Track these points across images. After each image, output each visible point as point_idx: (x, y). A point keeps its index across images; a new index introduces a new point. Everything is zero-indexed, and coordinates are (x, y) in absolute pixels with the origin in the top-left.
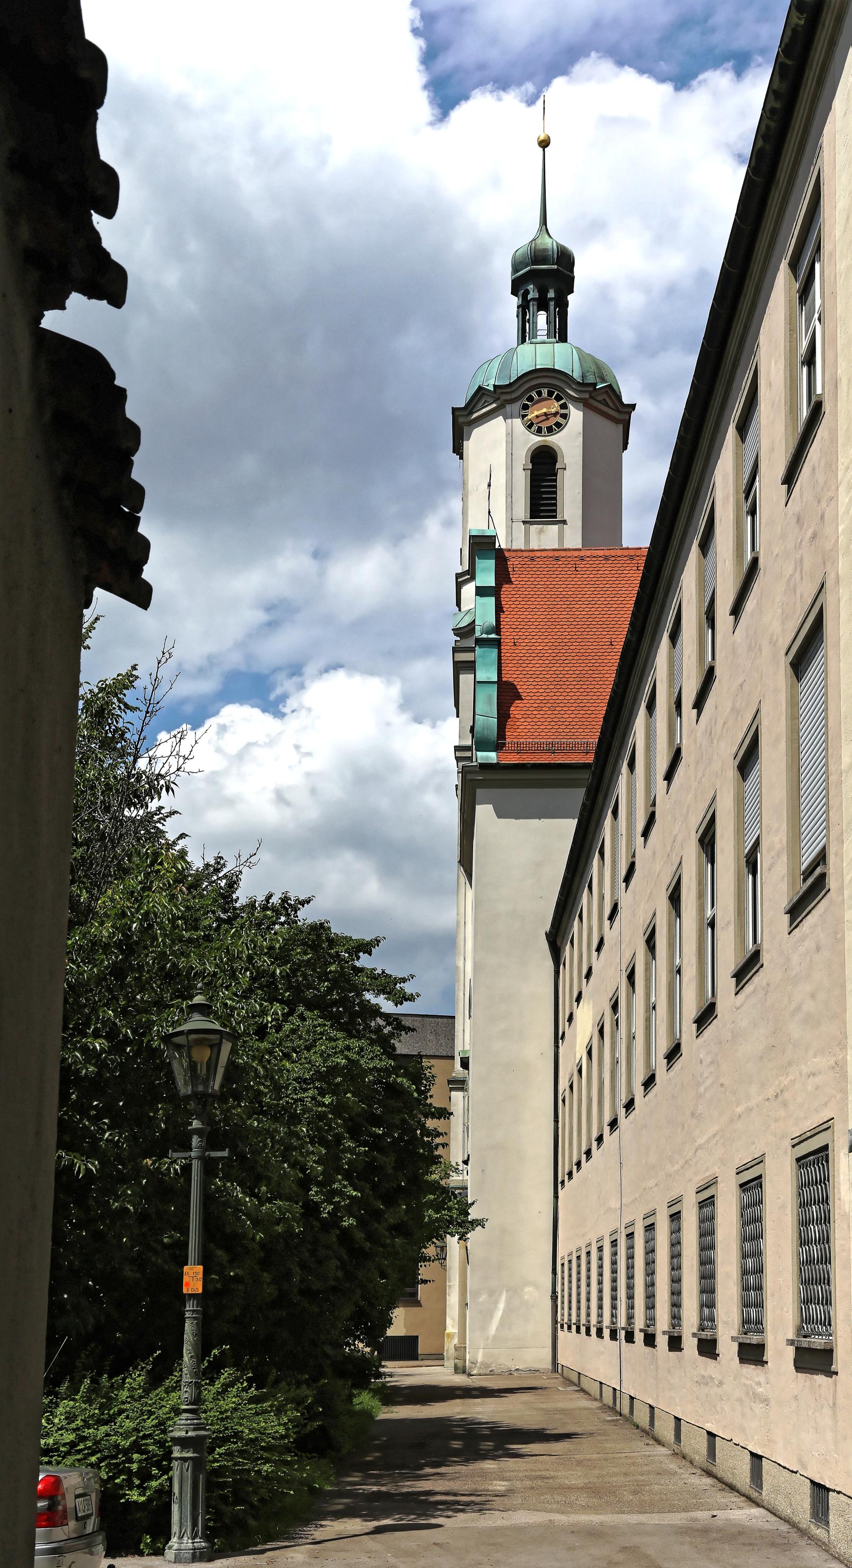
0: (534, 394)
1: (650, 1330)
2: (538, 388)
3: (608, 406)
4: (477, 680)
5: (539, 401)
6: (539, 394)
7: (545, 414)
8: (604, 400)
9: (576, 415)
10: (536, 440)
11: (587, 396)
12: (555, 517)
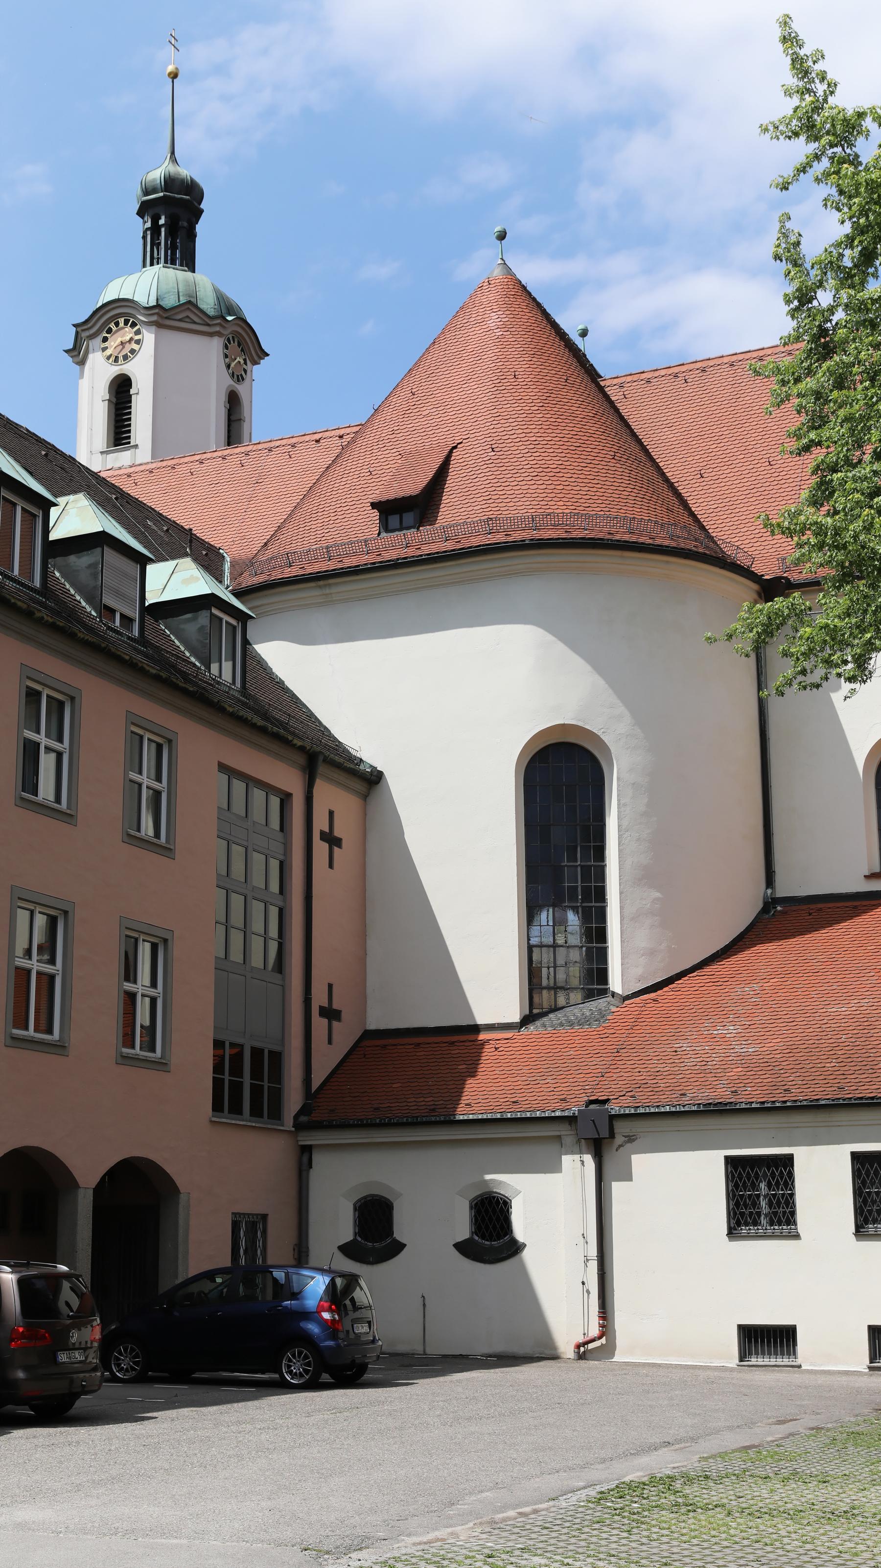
0: (112, 325)
1: (588, 1355)
2: (115, 319)
3: (195, 323)
4: (398, 527)
5: (116, 331)
6: (117, 324)
7: (122, 343)
8: (188, 317)
9: (149, 337)
10: (114, 371)
11: (155, 318)
12: (129, 443)
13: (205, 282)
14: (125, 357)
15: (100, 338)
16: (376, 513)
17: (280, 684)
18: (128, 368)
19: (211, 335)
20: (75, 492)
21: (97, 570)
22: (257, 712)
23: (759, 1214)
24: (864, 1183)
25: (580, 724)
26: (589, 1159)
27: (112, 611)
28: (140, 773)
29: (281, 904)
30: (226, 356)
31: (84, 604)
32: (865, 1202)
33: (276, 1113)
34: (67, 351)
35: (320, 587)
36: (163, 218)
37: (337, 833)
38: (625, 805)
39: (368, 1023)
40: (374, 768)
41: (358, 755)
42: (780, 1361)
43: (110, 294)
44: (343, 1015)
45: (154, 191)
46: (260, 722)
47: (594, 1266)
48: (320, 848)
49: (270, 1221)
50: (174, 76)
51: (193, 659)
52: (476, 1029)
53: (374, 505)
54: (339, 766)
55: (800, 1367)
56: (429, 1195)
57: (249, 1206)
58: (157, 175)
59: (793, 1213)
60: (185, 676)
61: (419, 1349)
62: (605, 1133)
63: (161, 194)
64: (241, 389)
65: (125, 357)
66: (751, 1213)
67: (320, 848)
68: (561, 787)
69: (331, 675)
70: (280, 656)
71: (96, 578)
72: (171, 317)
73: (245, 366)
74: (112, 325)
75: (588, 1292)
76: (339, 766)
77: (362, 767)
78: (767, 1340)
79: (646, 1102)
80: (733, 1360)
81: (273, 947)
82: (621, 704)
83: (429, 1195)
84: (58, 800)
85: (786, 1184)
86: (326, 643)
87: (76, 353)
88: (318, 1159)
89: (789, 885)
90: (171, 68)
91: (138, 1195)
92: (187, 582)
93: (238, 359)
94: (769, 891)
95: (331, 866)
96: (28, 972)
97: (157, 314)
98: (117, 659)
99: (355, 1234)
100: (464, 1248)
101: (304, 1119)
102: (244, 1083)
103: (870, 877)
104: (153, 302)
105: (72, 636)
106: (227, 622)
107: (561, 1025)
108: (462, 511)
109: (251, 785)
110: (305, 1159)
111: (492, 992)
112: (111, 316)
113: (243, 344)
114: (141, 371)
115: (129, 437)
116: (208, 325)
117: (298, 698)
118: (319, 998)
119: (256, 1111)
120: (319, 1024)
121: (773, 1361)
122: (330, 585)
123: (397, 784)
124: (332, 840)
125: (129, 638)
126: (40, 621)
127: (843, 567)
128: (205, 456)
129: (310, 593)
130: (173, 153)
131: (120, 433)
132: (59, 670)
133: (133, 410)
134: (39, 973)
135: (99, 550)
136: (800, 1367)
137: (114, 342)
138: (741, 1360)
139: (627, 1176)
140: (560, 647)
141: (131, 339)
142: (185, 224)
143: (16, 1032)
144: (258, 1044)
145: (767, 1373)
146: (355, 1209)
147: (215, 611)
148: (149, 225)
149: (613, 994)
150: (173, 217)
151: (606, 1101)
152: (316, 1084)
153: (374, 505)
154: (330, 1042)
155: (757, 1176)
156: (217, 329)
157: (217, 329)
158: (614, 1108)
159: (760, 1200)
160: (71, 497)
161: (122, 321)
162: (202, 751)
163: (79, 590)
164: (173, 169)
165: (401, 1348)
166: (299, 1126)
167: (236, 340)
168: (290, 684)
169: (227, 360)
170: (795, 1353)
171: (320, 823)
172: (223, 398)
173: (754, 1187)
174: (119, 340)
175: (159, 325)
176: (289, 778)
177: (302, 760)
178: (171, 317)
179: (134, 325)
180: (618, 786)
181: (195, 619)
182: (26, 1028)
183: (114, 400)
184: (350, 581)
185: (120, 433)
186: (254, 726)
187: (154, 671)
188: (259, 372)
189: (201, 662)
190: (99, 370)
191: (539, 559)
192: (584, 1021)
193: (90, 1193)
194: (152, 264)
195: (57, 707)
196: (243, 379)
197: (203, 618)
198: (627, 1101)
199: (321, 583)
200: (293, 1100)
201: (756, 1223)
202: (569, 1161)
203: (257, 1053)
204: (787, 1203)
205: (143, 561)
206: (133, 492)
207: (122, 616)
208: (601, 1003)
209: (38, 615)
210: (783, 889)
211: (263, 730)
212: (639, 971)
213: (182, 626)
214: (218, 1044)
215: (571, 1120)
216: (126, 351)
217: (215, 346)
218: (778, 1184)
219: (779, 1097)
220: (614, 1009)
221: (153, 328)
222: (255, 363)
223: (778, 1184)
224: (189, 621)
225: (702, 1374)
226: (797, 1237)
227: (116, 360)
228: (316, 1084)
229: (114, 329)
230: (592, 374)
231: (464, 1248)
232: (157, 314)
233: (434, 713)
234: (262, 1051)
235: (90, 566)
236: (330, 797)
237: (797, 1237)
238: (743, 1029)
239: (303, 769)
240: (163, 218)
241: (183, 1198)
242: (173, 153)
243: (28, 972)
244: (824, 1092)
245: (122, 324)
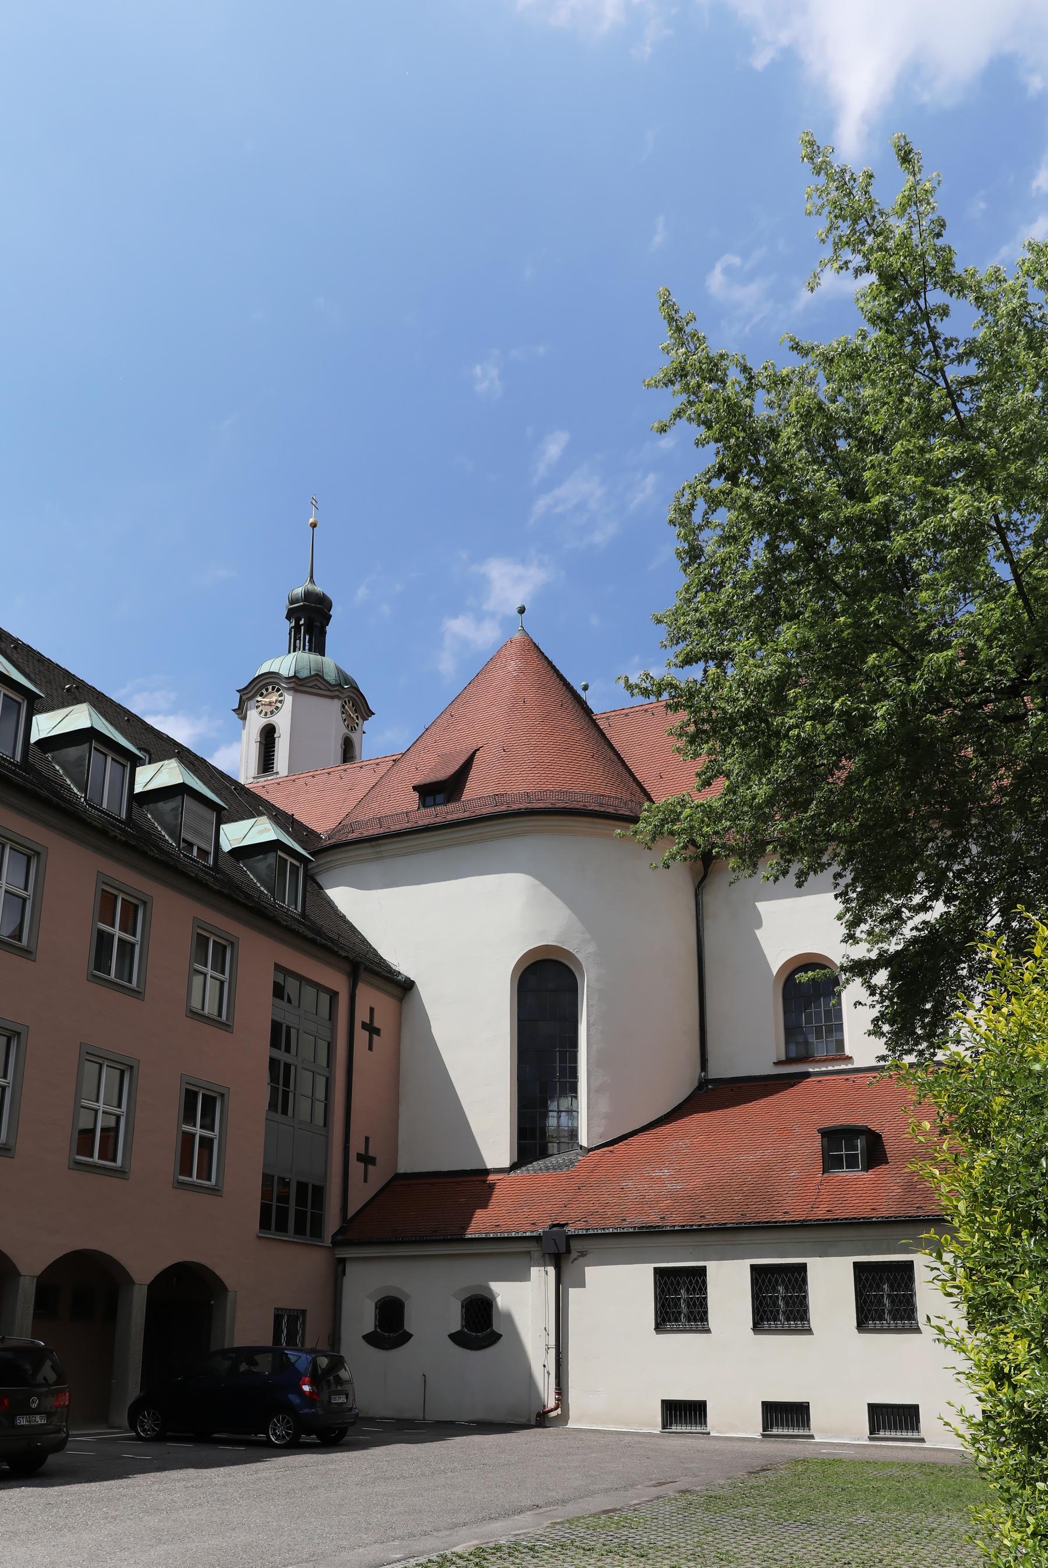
0: (264, 691)
9: (288, 698)
10: (263, 721)
11: (292, 685)
13: (329, 663)
16: (416, 795)
17: (343, 918)
18: (275, 720)
19: (332, 697)
20: (169, 758)
21: (178, 812)
22: (308, 927)
23: (680, 1313)
24: (760, 1289)
25: (559, 945)
26: (551, 1270)
27: (191, 845)
28: (206, 966)
29: (327, 1074)
31: (167, 837)
32: (761, 1304)
33: (317, 1231)
35: (373, 846)
37: (376, 1024)
38: (592, 1006)
39: (399, 1166)
40: (407, 979)
42: (694, 1429)
43: (264, 669)
44: (378, 1161)
45: (297, 601)
46: (311, 935)
47: (552, 1352)
48: (361, 1036)
49: (309, 1316)
50: (314, 525)
51: (262, 889)
52: (487, 1172)
53: (415, 788)
54: (378, 974)
55: (709, 1433)
56: (433, 1298)
57: (291, 1302)
58: (299, 591)
59: (706, 1313)
60: (248, 896)
61: (421, 1416)
62: (563, 1250)
64: (354, 736)
66: (771, 1312)
67: (361, 1036)
68: (545, 990)
69: (377, 911)
70: (345, 898)
71: (177, 818)
72: (304, 684)
74: (264, 691)
75: (549, 1373)
76: (378, 974)
77: (400, 978)
78: (684, 1413)
79: (596, 1225)
80: (658, 1429)
81: (320, 1107)
83: (433, 1298)
84: (220, 1015)
85: (700, 1290)
88: (350, 1268)
89: (718, 1070)
90: (311, 520)
91: (189, 1294)
92: (260, 832)
94: (703, 1074)
95: (370, 1048)
96: (193, 1135)
98: (288, 929)
99: (463, 1326)
100: (457, 1338)
101: (339, 1237)
102: (289, 1208)
103: (778, 1063)
104: (292, 674)
105: (143, 854)
107: (541, 1169)
108: (477, 790)
109: (303, 983)
110: (340, 1268)
111: (495, 1143)
112: (263, 684)
113: (358, 707)
114: (283, 721)
118: (357, 1146)
119: (300, 1230)
120: (356, 1168)
121: (688, 1429)
122: (380, 845)
123: (425, 990)
124: (372, 1030)
125: (204, 865)
126: (114, 839)
127: (1000, 1295)
129: (366, 851)
130: (312, 577)
131: (266, 763)
132: (132, 880)
134: (201, 1137)
135: (180, 797)
136: (709, 1433)
138: (664, 1428)
139: (582, 1284)
140: (544, 889)
143: (182, 1178)
144: (303, 1180)
145: (683, 1440)
146: (376, 1307)
148: (293, 624)
149: (581, 1147)
150: (311, 618)
151: (563, 1225)
152: (351, 1213)
153: (415, 788)
154: (365, 1181)
155: (678, 1283)
158: (571, 1230)
159: (680, 1303)
160: (166, 762)
161: (270, 688)
162: (259, 956)
163: (163, 828)
164: (310, 587)
165: (407, 1415)
166: (336, 1243)
168: (350, 918)
170: (705, 1423)
171: (362, 1015)
173: (676, 1292)
176: (335, 980)
178: (304, 684)
181: (265, 859)
182: (191, 1176)
185: (266, 763)
186: (305, 938)
187: (217, 888)
188: (367, 725)
190: (256, 721)
191: (530, 824)
192: (558, 1167)
193: (145, 1290)
194: (294, 651)
195: (220, 950)
197: (271, 858)
198: (581, 1225)
199: (374, 843)
200: (332, 1223)
201: (677, 1320)
202: (535, 1271)
203: (302, 1187)
204: (701, 1305)
205: (135, 762)
206: (265, 796)
207: (199, 848)
208: (572, 1155)
209: (112, 834)
210: (714, 1073)
211: (313, 941)
212: (601, 1130)
214: (267, 1179)
215: (538, 1239)
217: (337, 704)
218: (694, 1290)
219: (696, 1222)
220: (580, 1158)
222: (365, 719)
223: (694, 1290)
224: (260, 860)
225: (627, 1439)
226: (708, 1331)
228: (351, 1213)
230: (588, 712)
231: (457, 1338)
233: (454, 938)
234: (306, 1185)
235: (173, 809)
236: (369, 997)
237: (708, 1331)
238: (674, 1174)
241: (230, 1296)
242: (312, 577)
243: (193, 1135)
244: (729, 1218)
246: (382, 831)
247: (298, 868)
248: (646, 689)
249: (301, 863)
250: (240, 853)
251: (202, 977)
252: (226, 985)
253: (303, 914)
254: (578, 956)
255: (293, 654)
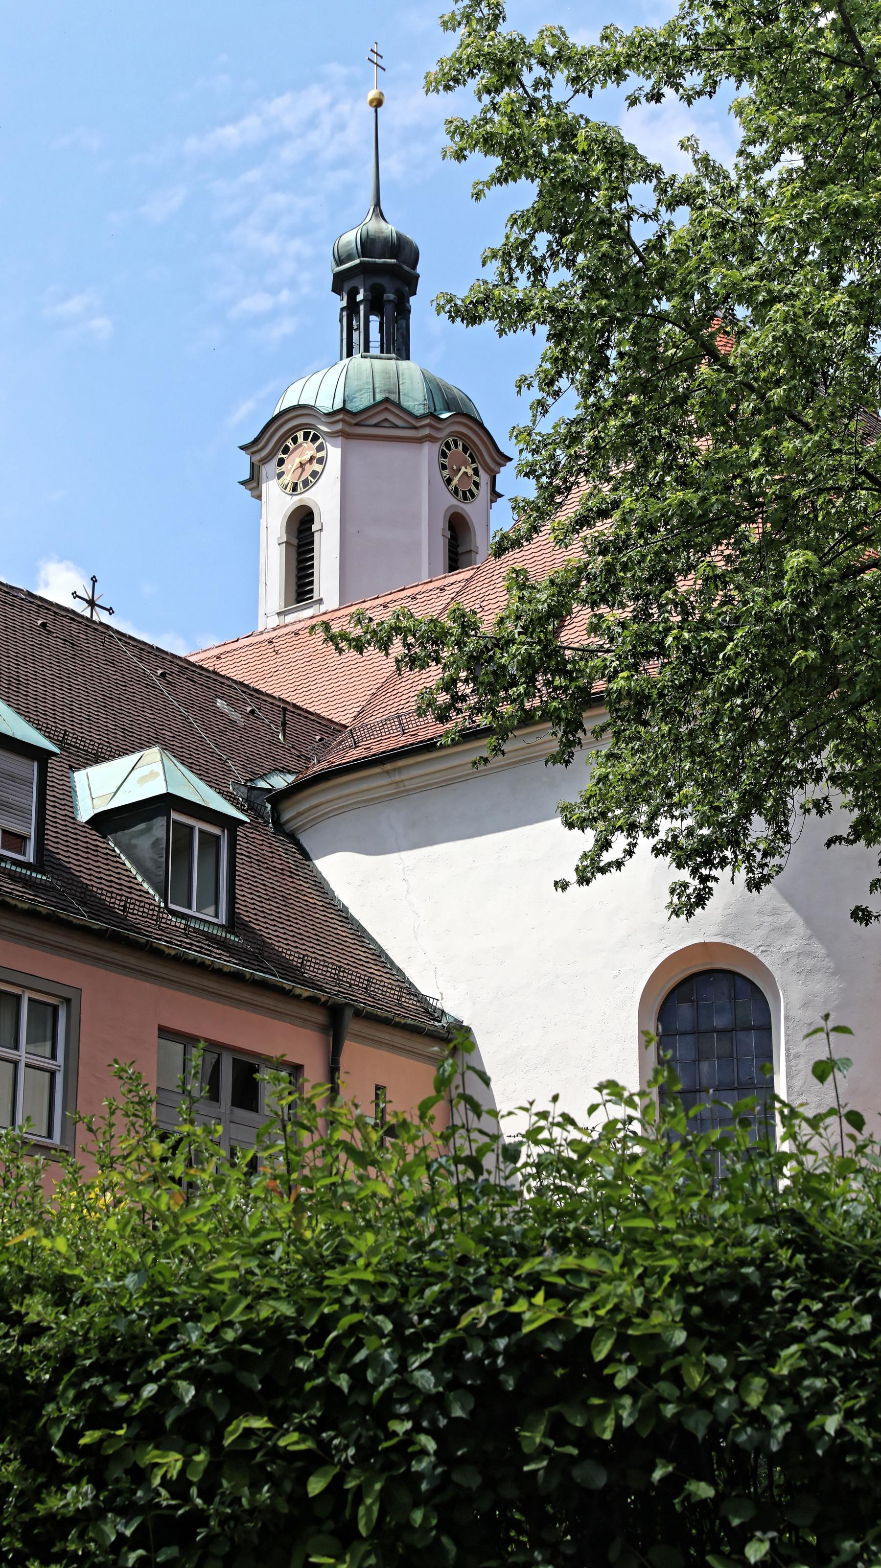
0: (289, 443)
3: (396, 427)
5: (295, 450)
7: (302, 465)
10: (291, 502)
11: (339, 426)
14: (306, 483)
15: (275, 461)
19: (420, 440)
25: (728, 941)
30: (444, 467)
34: (243, 483)
35: (387, 772)
36: (362, 291)
38: (797, 1056)
41: (439, 1006)
43: (289, 401)
45: (350, 258)
46: (231, 965)
50: (378, 103)
58: (351, 238)
63: (357, 261)
64: (471, 510)
65: (306, 483)
70: (341, 871)
72: (364, 423)
73: (475, 478)
74: (289, 443)
82: (789, 909)
86: (399, 850)
87: (254, 484)
90: (372, 94)
92: (143, 780)
93: (463, 469)
97: (342, 420)
104: (338, 405)
106: (201, 832)
114: (325, 499)
115: (311, 591)
116: (415, 428)
117: (364, 931)
128: (364, 605)
129: (375, 782)
130: (377, 204)
133: (316, 554)
137: (292, 462)
141: (312, 458)
142: (392, 296)
147: (174, 816)
148: (344, 303)
156: (427, 431)
157: (427, 431)
161: (300, 435)
164: (374, 226)
167: (460, 444)
169: (446, 472)
172: (441, 523)
174: (297, 461)
175: (345, 435)
176: (300, 1044)
177: (320, 1017)
179: (315, 438)
180: (787, 1028)
181: (148, 830)
183: (295, 542)
184: (417, 764)
189: (156, 889)
196: (473, 496)
199: (388, 767)
213: (134, 841)
216: (306, 474)
217: (426, 456)
221: (339, 440)
227: (294, 489)
229: (292, 447)
232: (342, 420)
239: (323, 1029)
240: (362, 291)
242: (377, 204)
245: (300, 440)
246: (402, 741)
247: (217, 838)
248: (358, 639)
249: (222, 827)
250: (108, 822)
251: (11, 1066)
252: (59, 1078)
253: (234, 923)
254: (765, 960)
255: (346, 361)
